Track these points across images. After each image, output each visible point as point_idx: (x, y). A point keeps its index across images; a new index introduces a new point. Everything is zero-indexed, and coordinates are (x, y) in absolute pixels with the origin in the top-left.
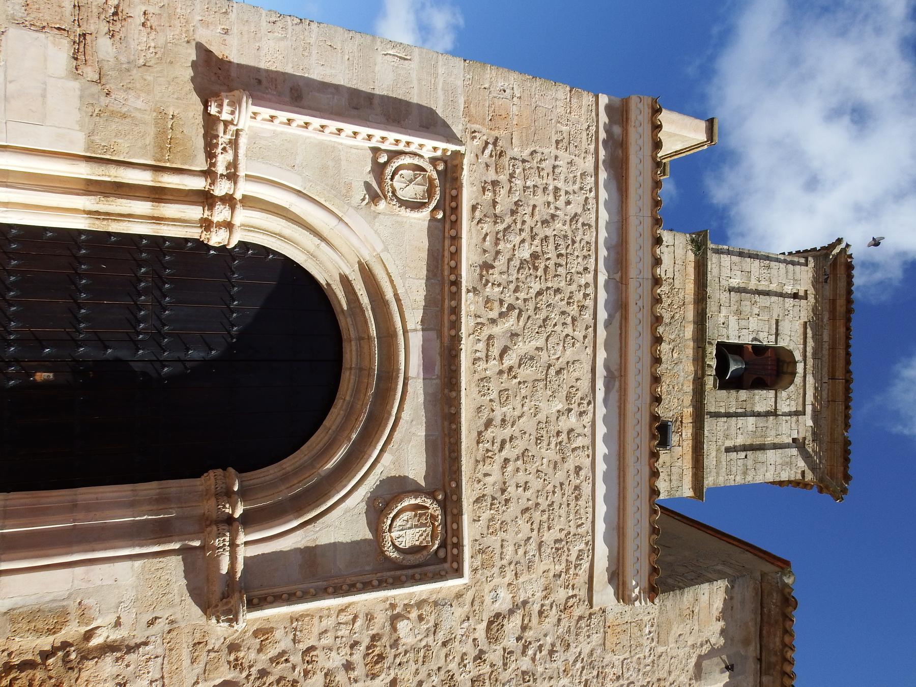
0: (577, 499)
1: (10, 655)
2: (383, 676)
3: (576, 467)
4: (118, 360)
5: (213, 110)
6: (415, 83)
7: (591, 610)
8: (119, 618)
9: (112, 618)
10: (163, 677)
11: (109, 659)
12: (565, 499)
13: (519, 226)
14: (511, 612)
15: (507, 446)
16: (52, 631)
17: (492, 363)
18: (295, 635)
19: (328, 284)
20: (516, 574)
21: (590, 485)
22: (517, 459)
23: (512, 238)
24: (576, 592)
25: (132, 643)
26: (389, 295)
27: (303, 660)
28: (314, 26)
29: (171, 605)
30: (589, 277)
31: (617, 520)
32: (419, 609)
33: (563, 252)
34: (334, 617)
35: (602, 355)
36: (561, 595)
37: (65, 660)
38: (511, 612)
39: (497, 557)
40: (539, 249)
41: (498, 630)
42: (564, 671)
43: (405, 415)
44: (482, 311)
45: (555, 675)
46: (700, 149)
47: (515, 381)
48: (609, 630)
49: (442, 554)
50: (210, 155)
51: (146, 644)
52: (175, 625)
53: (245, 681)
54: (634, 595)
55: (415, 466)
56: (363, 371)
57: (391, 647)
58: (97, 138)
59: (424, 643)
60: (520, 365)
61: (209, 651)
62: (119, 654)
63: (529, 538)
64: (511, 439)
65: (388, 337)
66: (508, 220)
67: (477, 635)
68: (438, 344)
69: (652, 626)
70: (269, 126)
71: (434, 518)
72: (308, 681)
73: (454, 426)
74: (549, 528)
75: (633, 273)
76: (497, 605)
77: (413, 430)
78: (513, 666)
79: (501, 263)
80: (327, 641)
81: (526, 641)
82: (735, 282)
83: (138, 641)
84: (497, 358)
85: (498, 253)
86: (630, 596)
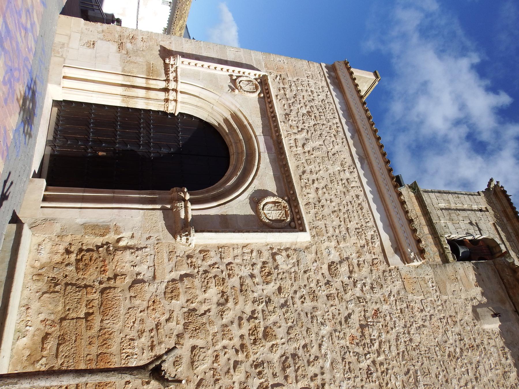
0: (361, 209)
1: (82, 244)
2: (272, 284)
3: (356, 195)
4: (132, 150)
5: (167, 61)
6: (243, 58)
7: (390, 268)
8: (133, 234)
9: (130, 234)
10: (154, 265)
11: (128, 252)
12: (355, 208)
13: (298, 102)
14: (341, 262)
15: (316, 182)
16: (102, 235)
17: (299, 149)
18: (221, 255)
19: (219, 124)
20: (338, 242)
21: (367, 204)
22: (323, 188)
23: (296, 105)
24: (376, 257)
25: (139, 247)
26: (246, 123)
27: (227, 268)
28: (202, 42)
29: (158, 231)
30: (337, 120)
31: (388, 222)
32: (286, 251)
33: (321, 111)
34: (241, 249)
35: (354, 150)
36: (368, 257)
37: (107, 250)
38: (341, 262)
39: (324, 232)
40: (310, 110)
41: (335, 270)
42: (384, 300)
43: (261, 166)
44: (289, 129)
45: (379, 301)
46: (375, 85)
47: (312, 156)
48: (404, 280)
49: (293, 224)
50: (167, 73)
51: (146, 248)
52: (160, 241)
53: (197, 274)
54: (412, 257)
55: (271, 186)
56: (239, 154)
57: (275, 269)
58: (126, 69)
59: (293, 270)
60: (313, 151)
61: (177, 256)
62: (133, 251)
63: (340, 225)
64: (317, 179)
65: (248, 140)
66: (293, 100)
67: (323, 272)
68: (272, 141)
69: (433, 282)
70: (188, 67)
71: (284, 207)
72: (231, 280)
73: (286, 169)
74: (350, 222)
75: (357, 117)
76: (331, 257)
77: (267, 172)
78: (350, 292)
79: (293, 113)
80: (238, 260)
81: (354, 280)
82: (442, 205)
83: (142, 246)
84: (301, 146)
85: (291, 110)
86: (410, 258)
